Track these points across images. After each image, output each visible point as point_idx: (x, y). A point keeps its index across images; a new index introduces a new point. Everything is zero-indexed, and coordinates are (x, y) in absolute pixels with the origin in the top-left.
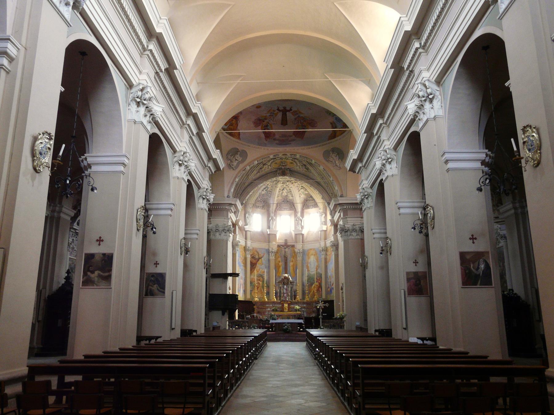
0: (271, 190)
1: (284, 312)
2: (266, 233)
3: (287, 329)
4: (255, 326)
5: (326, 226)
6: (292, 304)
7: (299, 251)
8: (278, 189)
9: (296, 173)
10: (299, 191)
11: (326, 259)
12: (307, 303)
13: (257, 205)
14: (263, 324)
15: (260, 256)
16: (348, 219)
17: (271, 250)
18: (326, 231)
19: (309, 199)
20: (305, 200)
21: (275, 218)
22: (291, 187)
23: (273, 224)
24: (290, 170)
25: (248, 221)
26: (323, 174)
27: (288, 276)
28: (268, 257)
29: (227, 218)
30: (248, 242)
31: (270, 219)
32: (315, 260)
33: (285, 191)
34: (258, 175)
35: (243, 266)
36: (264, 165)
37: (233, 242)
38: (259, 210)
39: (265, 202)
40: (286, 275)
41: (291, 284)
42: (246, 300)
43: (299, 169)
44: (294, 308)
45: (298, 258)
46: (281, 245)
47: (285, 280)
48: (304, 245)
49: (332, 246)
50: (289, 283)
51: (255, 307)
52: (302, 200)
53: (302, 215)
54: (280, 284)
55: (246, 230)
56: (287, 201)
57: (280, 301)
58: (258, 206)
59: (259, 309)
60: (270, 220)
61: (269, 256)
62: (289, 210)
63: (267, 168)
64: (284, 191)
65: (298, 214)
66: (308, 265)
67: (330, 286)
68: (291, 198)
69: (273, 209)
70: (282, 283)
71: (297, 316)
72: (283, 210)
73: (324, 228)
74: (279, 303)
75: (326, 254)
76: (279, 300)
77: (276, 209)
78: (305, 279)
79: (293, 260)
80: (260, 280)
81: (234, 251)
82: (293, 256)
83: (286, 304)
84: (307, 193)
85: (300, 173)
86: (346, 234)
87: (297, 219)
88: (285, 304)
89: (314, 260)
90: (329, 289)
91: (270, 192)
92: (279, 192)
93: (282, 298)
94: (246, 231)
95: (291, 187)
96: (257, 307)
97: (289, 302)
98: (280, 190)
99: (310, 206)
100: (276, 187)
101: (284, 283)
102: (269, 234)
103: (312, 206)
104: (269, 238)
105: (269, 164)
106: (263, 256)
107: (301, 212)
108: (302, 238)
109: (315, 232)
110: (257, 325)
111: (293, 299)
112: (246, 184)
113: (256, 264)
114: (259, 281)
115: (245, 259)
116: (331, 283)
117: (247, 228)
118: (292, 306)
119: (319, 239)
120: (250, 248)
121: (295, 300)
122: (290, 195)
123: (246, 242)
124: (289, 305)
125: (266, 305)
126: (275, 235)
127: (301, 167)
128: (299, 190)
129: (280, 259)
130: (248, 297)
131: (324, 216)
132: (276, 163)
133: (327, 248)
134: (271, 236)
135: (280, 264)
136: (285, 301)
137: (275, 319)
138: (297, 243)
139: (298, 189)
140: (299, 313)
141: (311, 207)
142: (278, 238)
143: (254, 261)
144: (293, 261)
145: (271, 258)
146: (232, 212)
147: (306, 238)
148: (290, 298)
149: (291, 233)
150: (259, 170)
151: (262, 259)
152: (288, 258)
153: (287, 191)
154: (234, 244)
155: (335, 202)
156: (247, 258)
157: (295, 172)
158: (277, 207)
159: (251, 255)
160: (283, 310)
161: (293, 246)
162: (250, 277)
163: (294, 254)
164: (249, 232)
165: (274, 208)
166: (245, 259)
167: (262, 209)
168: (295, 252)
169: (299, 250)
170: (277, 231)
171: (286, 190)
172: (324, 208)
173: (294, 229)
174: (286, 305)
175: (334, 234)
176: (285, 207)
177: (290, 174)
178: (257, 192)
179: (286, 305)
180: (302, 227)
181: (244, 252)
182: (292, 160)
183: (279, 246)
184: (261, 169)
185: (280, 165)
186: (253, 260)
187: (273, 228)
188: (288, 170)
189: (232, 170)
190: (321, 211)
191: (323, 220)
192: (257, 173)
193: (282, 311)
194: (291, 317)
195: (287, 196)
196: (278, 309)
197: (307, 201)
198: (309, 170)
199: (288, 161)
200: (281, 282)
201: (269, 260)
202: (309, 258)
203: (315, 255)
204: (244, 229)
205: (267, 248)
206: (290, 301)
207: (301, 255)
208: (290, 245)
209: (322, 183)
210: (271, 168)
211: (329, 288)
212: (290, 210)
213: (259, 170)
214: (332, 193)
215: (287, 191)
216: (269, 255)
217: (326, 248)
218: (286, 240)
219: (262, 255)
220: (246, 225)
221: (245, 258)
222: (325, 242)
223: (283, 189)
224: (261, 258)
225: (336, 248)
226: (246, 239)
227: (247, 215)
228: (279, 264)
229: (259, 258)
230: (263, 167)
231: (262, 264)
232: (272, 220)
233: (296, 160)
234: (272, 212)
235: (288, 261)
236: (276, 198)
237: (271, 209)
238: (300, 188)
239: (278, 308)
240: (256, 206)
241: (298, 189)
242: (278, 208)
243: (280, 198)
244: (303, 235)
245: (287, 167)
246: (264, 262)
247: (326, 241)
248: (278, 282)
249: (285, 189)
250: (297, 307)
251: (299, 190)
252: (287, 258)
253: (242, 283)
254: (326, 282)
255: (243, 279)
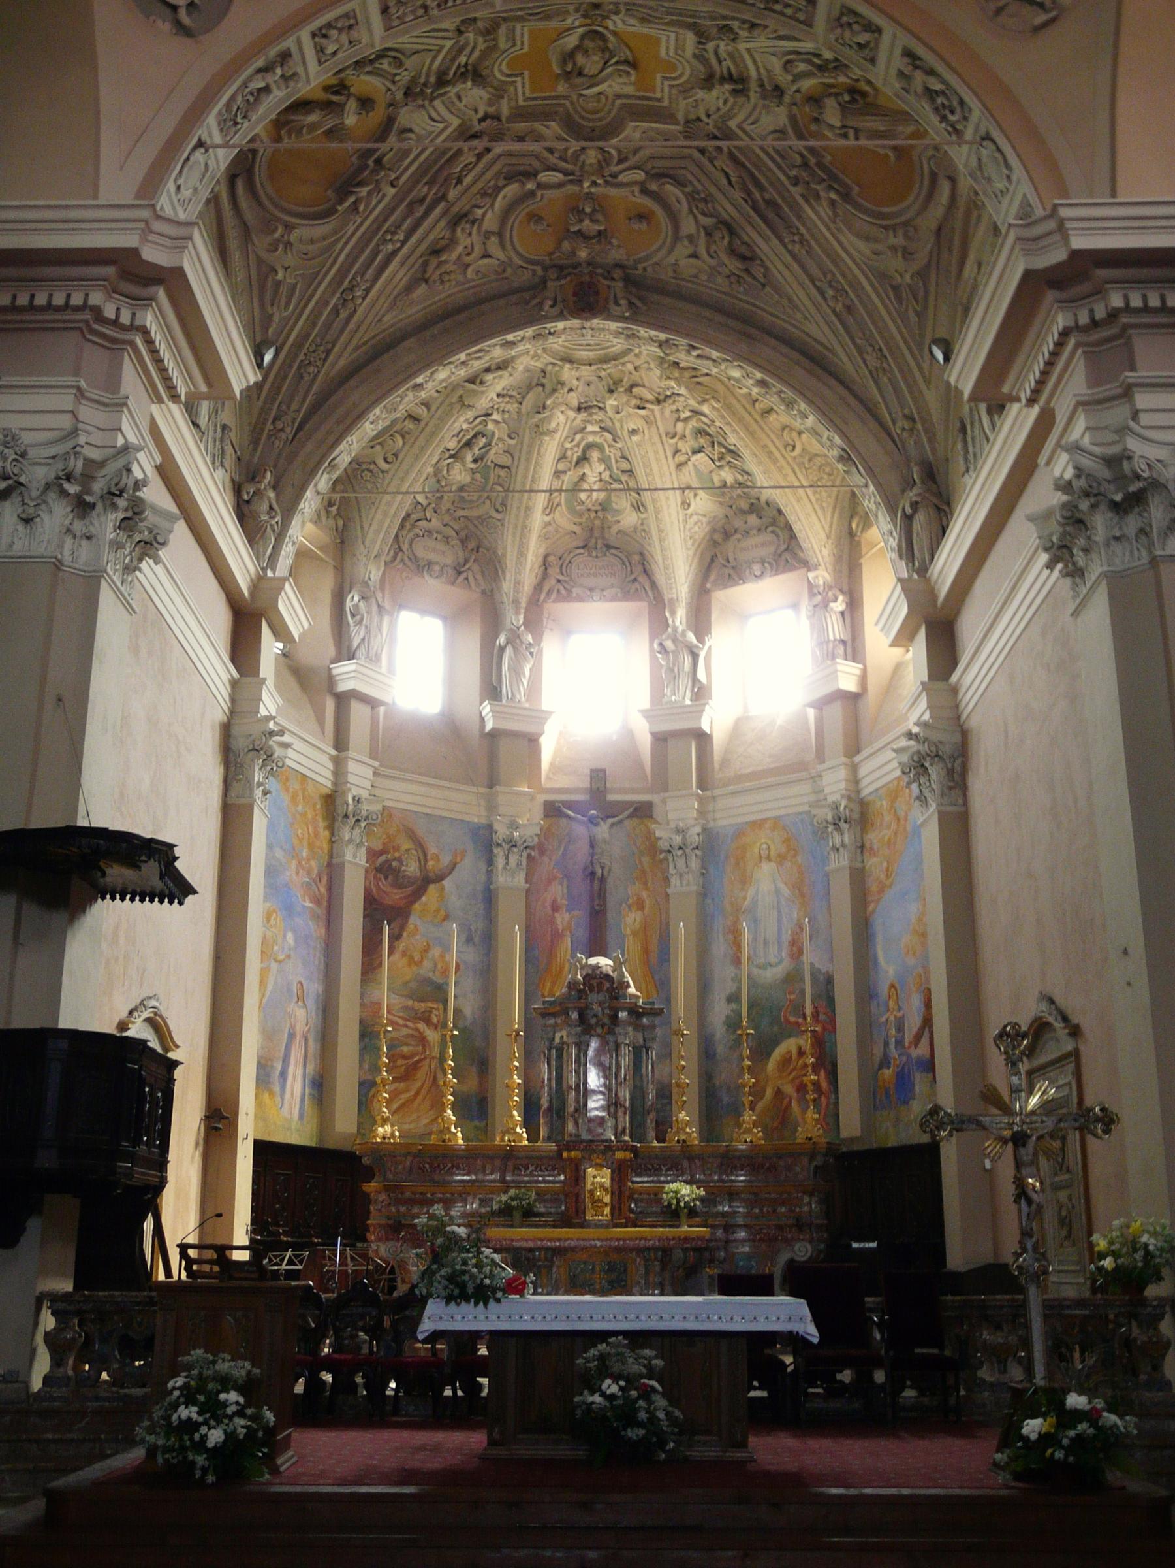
0: (505, 460)
1: (583, 1224)
2: (476, 731)
3: (627, 1415)
4: (226, 1382)
5: (855, 669)
6: (642, 1170)
7: (678, 839)
8: (550, 449)
9: (669, 294)
10: (680, 466)
11: (858, 877)
12: (753, 1161)
13: (420, 552)
14: (375, 1331)
15: (431, 863)
16: (1142, 400)
17: (501, 830)
18: (852, 699)
19: (738, 523)
20: (714, 530)
21: (530, 639)
22: (634, 432)
23: (516, 672)
24: (629, 281)
25: (356, 635)
26: (855, 285)
27: (617, 967)
28: (482, 877)
29: (105, 397)
30: (352, 766)
31: (502, 640)
32: (786, 891)
33: (594, 471)
34: (422, 301)
35: (315, 917)
36: (458, 220)
37: (235, 731)
38: (432, 584)
39: (472, 545)
40: (604, 962)
41: (638, 1027)
42: (330, 1144)
43: (688, 266)
44: (656, 1195)
45: (674, 881)
46: (569, 805)
47: (593, 997)
48: (714, 798)
49: (918, 767)
50: (623, 1015)
51: (371, 1187)
52: (700, 531)
53: (700, 622)
54: (555, 1028)
55: (343, 686)
56: (608, 547)
57: (553, 1146)
58: (430, 564)
59: (398, 1202)
60: (502, 649)
61: (490, 873)
62: (614, 599)
63: (478, 250)
64: (587, 470)
65: (673, 613)
66: (736, 922)
67: (893, 1052)
68: (629, 519)
69: (517, 583)
70: (575, 1015)
71: (678, 1255)
72: (580, 599)
73: (847, 678)
74: (554, 1162)
75: (862, 847)
76: (549, 1139)
77: (538, 588)
78: (720, 1011)
79: (644, 894)
80: (428, 1022)
81: (236, 788)
82: (644, 872)
83: (599, 1166)
84: (730, 480)
85: (696, 300)
86: (1132, 524)
87: (669, 644)
88: (591, 1171)
89: (777, 891)
90: (887, 1073)
91: (503, 473)
92: (558, 474)
93: (570, 1127)
94: (343, 700)
95: (634, 432)
96: (387, 1189)
97: (619, 1155)
98: (563, 457)
99: (750, 563)
100: (539, 431)
101: (582, 1019)
102: (494, 735)
103: (763, 562)
104: (492, 758)
105: (490, 221)
106: (453, 866)
107: (690, 605)
108: (699, 758)
109: (780, 721)
110: (240, 1369)
111: (651, 1134)
112: (340, 360)
113: (399, 915)
114: (422, 1026)
115: (332, 872)
116: (900, 1028)
117: (348, 675)
118: (641, 1182)
119: (811, 756)
120: (365, 807)
121: (661, 1139)
122: (622, 503)
123: (339, 765)
124: (620, 1173)
125: (450, 1172)
126: (532, 741)
127: (702, 251)
128: (681, 458)
129: (557, 891)
130: (345, 1124)
131: (840, 605)
132: (534, 217)
133: (864, 805)
134: (503, 746)
135: (562, 919)
136: (595, 1149)
137: (482, 1295)
138: (666, 790)
139: (677, 452)
140: (700, 1238)
141: (757, 569)
142: (552, 765)
143: (394, 896)
144: (640, 905)
145: (502, 880)
146: (175, 397)
147: (725, 762)
148: (625, 1120)
149: (629, 735)
150: (425, 264)
151: (446, 883)
152: (610, 882)
153: (609, 468)
154: (240, 743)
155: (1026, 252)
156: (341, 866)
157: (661, 289)
158: (545, 575)
159: (372, 855)
160: (580, 1211)
161: (643, 811)
162: (362, 995)
163: (646, 860)
164: (365, 710)
165: (529, 579)
166: (332, 872)
167: (453, 584)
168: (652, 847)
169: (678, 831)
170: (542, 717)
171: (601, 460)
172: (838, 559)
173: (646, 704)
174: (598, 1178)
175: (931, 676)
176: (591, 582)
177: (631, 304)
178: (417, 458)
179: (598, 1178)
180: (701, 693)
181: (321, 824)
182: (645, 191)
183: (553, 810)
184: (436, 252)
185: (568, 234)
186: (385, 885)
187: (521, 696)
188: (617, 274)
189: (166, 27)
190: (822, 576)
191: (836, 629)
192: (409, 289)
193: (572, 1217)
194: (637, 1267)
195: (604, 507)
196: (540, 1208)
197: (727, 535)
198: (758, 272)
199: (612, 192)
200: (565, 1012)
201: (489, 898)
202: (745, 881)
203: (781, 859)
204: (331, 680)
205: (476, 815)
206: (626, 1148)
207: (695, 864)
208: (626, 805)
209: (845, 359)
210: (500, 254)
211: (885, 1062)
212: (627, 596)
213: (425, 264)
214: (910, 418)
215: (609, 468)
216: (490, 862)
217: (856, 808)
218: (598, 776)
219: (446, 860)
220: (345, 652)
221: (329, 865)
222: (854, 769)
223: (583, 459)
224: (440, 878)
225: (950, 772)
226: (340, 742)
227: (353, 600)
228: (552, 921)
229: (426, 881)
230: (453, 241)
231: (447, 917)
232: (515, 649)
233: (671, 190)
234: (516, 602)
235: (611, 902)
236: (538, 519)
237: (507, 586)
238: (685, 447)
239: (540, 1194)
240: (415, 559)
241: (677, 452)
242: (550, 583)
243: (563, 518)
244: (702, 738)
245: (616, 254)
246: (455, 902)
247: (858, 759)
248: (545, 1014)
249: (595, 455)
250: (686, 1191)
251: (681, 458)
252: (602, 880)
253: (300, 1028)
254: (866, 1026)
255: (311, 1002)
